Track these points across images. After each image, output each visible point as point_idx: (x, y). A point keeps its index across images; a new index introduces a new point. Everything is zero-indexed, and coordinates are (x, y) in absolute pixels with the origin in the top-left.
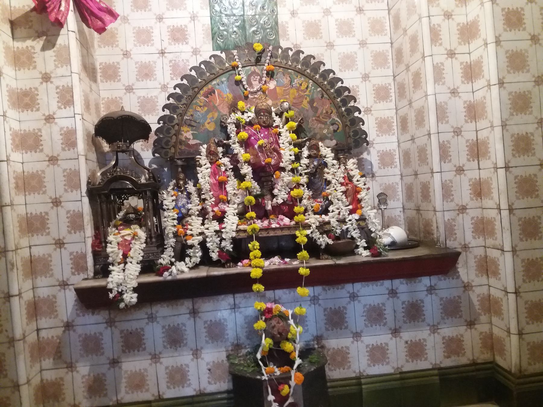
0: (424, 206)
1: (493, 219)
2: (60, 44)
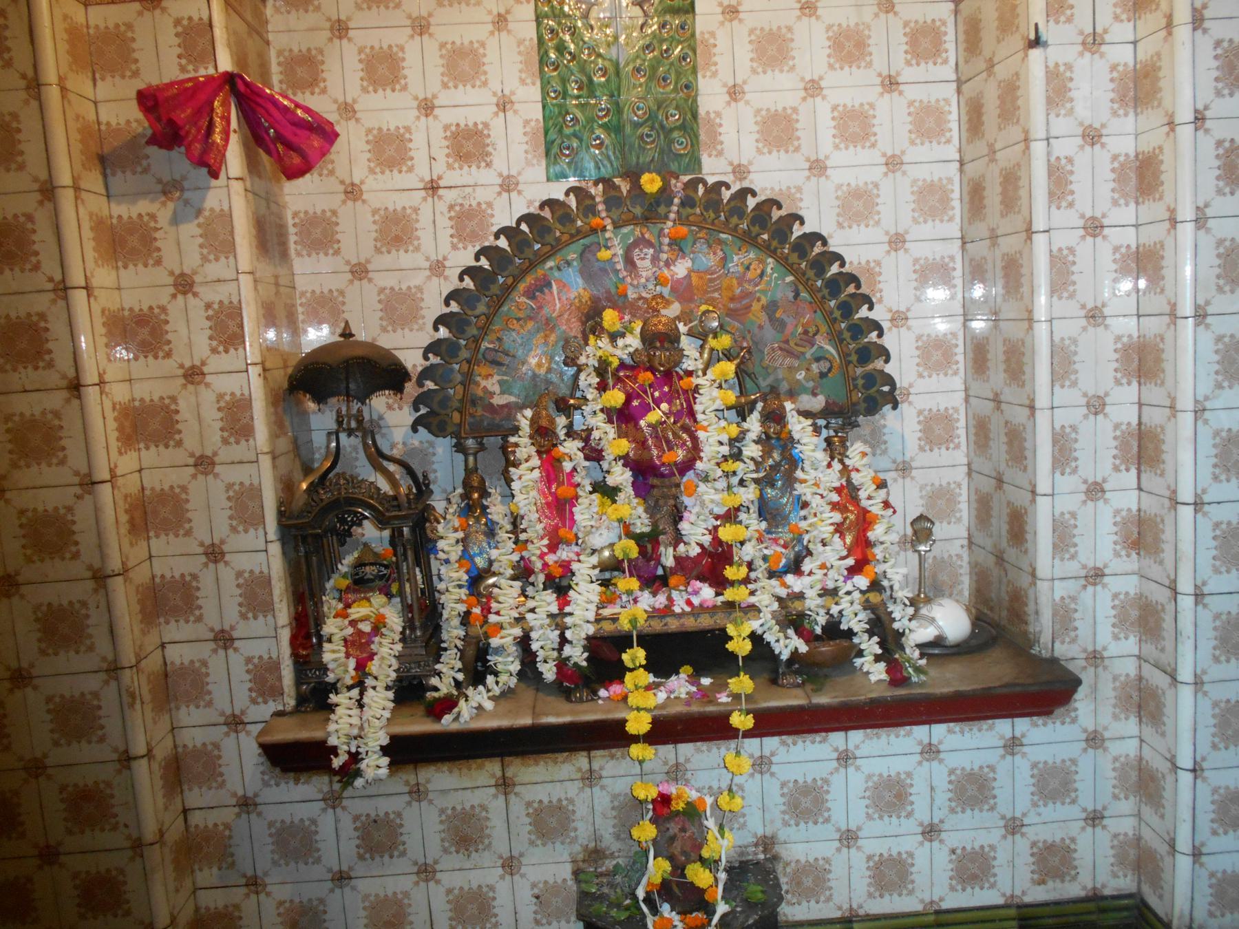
0: (1011, 554)
1: (1160, 607)
2: (212, 210)
